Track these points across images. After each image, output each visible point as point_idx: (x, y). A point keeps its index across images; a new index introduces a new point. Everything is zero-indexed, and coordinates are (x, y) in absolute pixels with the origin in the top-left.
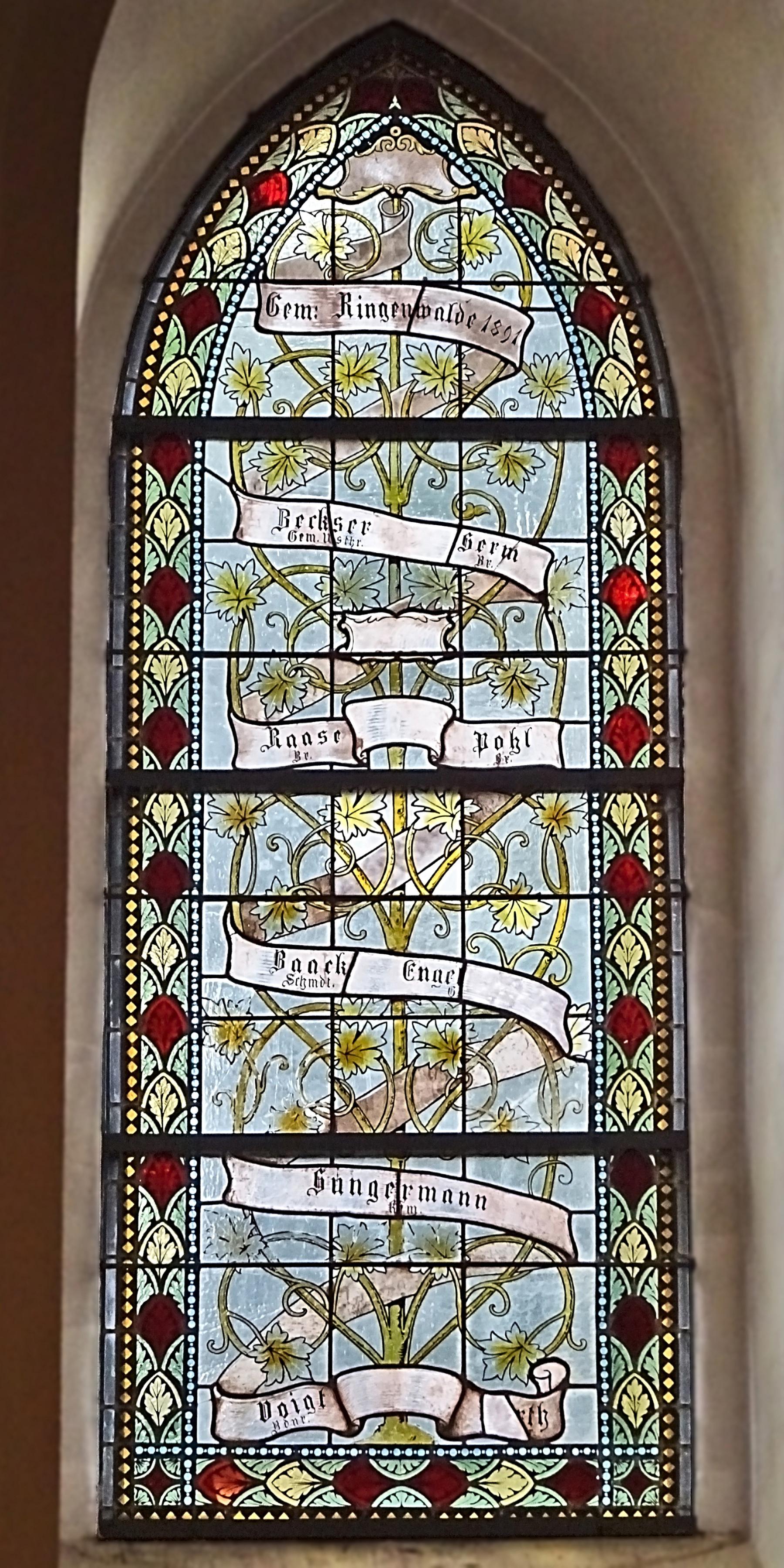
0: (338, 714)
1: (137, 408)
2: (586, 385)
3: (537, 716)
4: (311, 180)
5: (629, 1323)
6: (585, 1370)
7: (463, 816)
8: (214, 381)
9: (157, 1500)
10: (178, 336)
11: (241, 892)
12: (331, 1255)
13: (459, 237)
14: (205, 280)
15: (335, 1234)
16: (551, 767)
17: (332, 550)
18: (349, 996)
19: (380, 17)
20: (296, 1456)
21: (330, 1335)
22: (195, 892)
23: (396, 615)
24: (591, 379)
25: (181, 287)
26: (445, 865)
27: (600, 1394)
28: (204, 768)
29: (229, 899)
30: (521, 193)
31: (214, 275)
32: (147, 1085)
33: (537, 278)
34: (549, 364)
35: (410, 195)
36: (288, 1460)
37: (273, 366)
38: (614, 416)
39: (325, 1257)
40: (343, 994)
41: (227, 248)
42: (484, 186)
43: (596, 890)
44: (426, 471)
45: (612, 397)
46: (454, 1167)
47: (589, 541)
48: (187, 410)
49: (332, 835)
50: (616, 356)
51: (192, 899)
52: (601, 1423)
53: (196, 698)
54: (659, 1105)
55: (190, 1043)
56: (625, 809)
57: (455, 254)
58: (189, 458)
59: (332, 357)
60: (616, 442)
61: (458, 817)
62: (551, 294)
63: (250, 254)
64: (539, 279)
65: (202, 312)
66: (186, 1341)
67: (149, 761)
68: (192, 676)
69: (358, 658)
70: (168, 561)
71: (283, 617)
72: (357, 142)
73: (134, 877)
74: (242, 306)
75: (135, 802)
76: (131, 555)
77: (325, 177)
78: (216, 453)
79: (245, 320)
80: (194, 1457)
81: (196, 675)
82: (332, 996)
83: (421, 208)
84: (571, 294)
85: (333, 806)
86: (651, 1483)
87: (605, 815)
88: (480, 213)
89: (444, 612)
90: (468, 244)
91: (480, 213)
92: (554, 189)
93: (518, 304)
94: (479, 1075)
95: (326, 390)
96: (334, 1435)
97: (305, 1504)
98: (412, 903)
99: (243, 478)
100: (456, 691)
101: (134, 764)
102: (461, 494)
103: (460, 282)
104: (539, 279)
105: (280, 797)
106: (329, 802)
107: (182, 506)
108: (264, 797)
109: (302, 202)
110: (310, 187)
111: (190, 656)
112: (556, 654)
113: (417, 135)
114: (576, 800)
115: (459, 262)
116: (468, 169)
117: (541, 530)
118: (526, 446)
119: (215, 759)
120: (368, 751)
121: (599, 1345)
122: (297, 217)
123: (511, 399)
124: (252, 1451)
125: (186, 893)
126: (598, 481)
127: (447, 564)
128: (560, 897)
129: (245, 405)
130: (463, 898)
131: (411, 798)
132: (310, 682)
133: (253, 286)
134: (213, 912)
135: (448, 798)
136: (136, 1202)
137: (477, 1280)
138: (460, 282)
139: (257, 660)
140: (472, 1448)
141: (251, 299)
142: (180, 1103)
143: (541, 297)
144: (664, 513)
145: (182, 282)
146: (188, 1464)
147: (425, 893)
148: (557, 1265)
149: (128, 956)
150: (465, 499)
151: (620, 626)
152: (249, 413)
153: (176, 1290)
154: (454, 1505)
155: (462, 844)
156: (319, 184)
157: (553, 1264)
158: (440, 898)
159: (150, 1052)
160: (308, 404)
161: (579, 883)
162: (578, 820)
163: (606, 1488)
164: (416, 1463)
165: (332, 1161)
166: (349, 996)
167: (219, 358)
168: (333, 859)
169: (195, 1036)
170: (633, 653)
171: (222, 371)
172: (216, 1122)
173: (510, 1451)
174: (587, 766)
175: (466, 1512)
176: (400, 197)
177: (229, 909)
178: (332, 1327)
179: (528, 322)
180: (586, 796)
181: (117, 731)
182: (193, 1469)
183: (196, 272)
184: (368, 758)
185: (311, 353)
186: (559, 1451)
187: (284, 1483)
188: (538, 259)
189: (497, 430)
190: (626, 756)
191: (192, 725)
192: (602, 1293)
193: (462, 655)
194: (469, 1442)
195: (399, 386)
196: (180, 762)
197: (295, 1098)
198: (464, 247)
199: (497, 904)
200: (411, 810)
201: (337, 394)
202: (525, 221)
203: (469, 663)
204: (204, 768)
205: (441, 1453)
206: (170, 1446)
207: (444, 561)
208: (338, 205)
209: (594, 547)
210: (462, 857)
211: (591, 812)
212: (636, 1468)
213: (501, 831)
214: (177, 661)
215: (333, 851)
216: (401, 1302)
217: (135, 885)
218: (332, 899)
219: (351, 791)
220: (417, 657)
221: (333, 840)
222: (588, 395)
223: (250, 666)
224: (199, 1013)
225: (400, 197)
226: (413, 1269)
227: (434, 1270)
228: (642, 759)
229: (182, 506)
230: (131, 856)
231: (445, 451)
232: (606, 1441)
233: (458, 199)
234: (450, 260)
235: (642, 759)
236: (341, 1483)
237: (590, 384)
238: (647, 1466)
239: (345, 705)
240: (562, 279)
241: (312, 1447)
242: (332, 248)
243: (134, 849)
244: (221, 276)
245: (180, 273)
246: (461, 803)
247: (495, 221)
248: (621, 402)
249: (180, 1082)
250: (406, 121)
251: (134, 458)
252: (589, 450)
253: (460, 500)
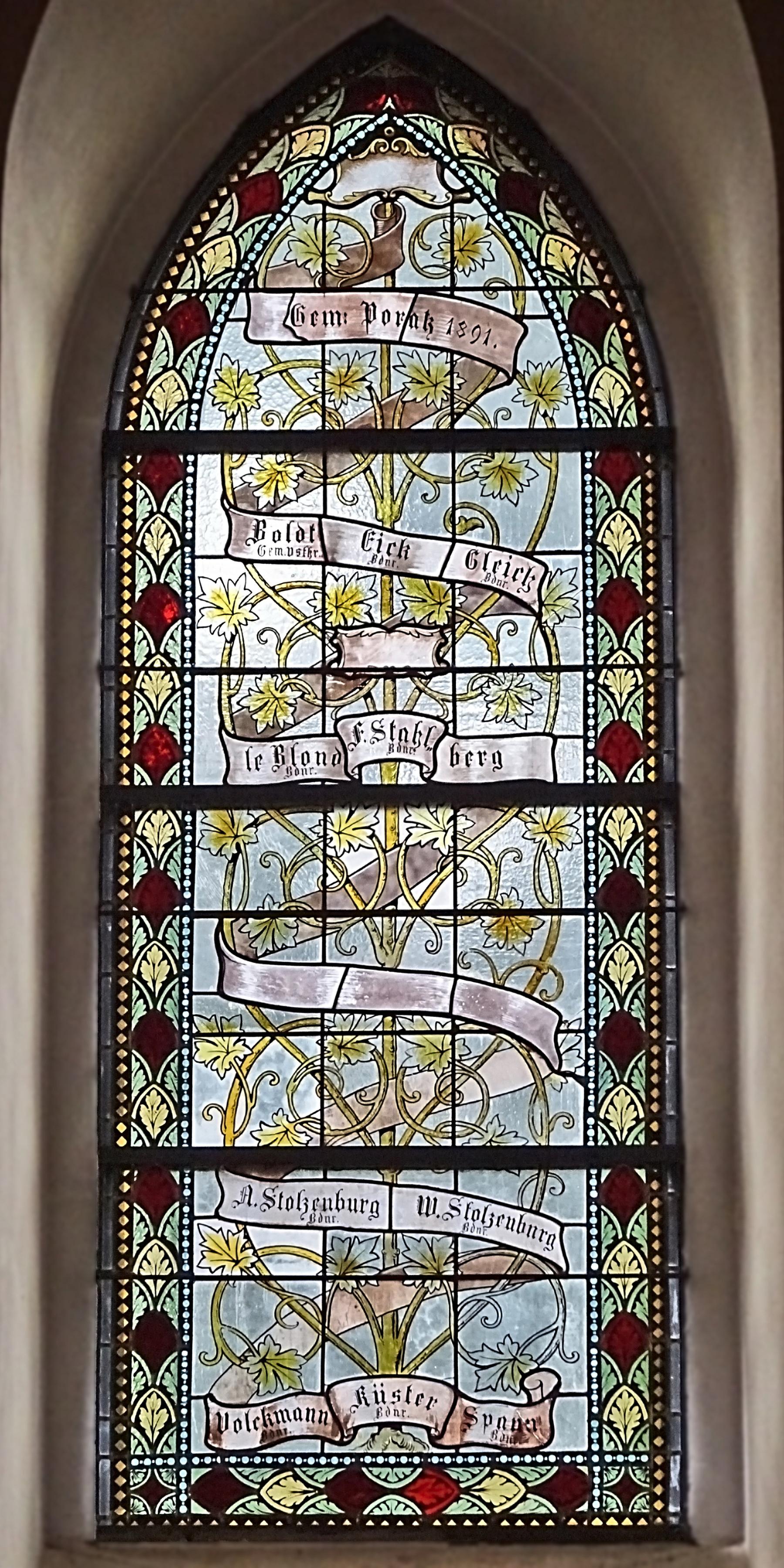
0: (330, 729)
1: (126, 421)
2: (580, 394)
3: (529, 731)
4: (300, 184)
5: (620, 1340)
6: (575, 1379)
7: (455, 832)
8: (202, 392)
9: (153, 1510)
10: (167, 349)
11: (234, 908)
12: (325, 1267)
13: (452, 242)
14: (193, 291)
15: (328, 1248)
16: (544, 782)
17: (324, 564)
18: (341, 1012)
19: (371, 19)
20: (289, 1466)
21: (323, 1346)
22: (186, 908)
23: (390, 631)
24: (586, 389)
25: (169, 300)
26: (438, 881)
27: (591, 1404)
28: (195, 783)
29: (220, 915)
30: (514, 197)
31: (204, 283)
32: (138, 1252)
33: (530, 283)
34: (550, 374)
35: (403, 200)
36: (283, 1468)
37: (262, 378)
38: (609, 425)
39: (316, 1270)
40: (334, 1010)
41: (217, 257)
42: (478, 190)
43: (591, 906)
44: (421, 486)
45: (607, 406)
46: (446, 1180)
47: (583, 553)
48: (175, 423)
49: (324, 850)
50: (611, 365)
51: (183, 914)
52: (590, 1430)
53: (187, 714)
54: (655, 1420)
55: (181, 1058)
56: (621, 824)
57: (448, 258)
58: (181, 474)
59: (323, 367)
60: (612, 454)
61: (451, 833)
62: (545, 302)
63: (239, 263)
64: (532, 284)
65: (192, 324)
66: (180, 982)
67: (141, 777)
68: (184, 690)
69: (350, 674)
70: (155, 1305)
71: (276, 632)
72: (351, 142)
73: (126, 608)
74: (231, 316)
75: (127, 820)
76: (121, 574)
77: (315, 180)
78: (208, 465)
79: (234, 330)
80: (189, 1467)
81: (185, 979)
82: (323, 1011)
83: (414, 215)
84: (566, 299)
85: (325, 821)
86: (641, 1489)
87: (601, 830)
88: (473, 219)
89: (436, 627)
90: (461, 250)
91: (473, 219)
92: (548, 193)
93: (512, 312)
94: (470, 1090)
95: (315, 401)
96: (326, 1444)
97: (299, 1512)
98: (403, 919)
99: (232, 721)
100: (450, 706)
101: (126, 782)
102: (454, 509)
103: (453, 288)
104: (532, 284)
105: (272, 812)
106: (321, 816)
107: (168, 1395)
108: (257, 813)
109: (293, 207)
110: (300, 191)
111: (181, 672)
112: (550, 668)
113: (411, 137)
114: (570, 814)
115: (452, 268)
116: (462, 173)
117: (536, 539)
118: (520, 456)
119: (207, 771)
120: (360, 767)
121: (590, 1356)
122: (287, 222)
123: (506, 408)
124: (245, 1460)
125: (177, 909)
126: (595, 705)
127: (440, 578)
128: (551, 912)
129: (233, 417)
130: (455, 912)
131: (403, 814)
132: (302, 697)
133: (242, 295)
134: (205, 928)
135: (440, 815)
136: (132, 635)
137: (470, 1293)
138: (453, 288)
139: (246, 677)
140: (465, 1455)
141: (240, 310)
142: (170, 1418)
143: (533, 303)
144: (659, 533)
145: (169, 295)
146: (183, 1473)
147: (416, 907)
148: (549, 1277)
149: (120, 974)
150: (458, 513)
151: (615, 639)
152: (238, 427)
153: (171, 1308)
154: (447, 1512)
155: (455, 860)
156: (310, 188)
157: (544, 1277)
158: (434, 913)
159: (142, 1219)
160: (300, 415)
161: (575, 898)
162: (573, 836)
163: (596, 1493)
164: (407, 1471)
165: (325, 1174)
166: (341, 1012)
167: (208, 369)
168: (325, 875)
169: (188, 621)
170: (630, 667)
171: (210, 384)
172: (206, 1134)
173: (504, 1459)
174: (580, 1143)
175: (460, 1519)
176: (392, 200)
177: (221, 924)
178: (325, 1339)
179: (522, 330)
180: (581, 811)
181: (104, 1510)
182: (188, 1479)
183: (185, 284)
184: (360, 774)
185: (304, 363)
186: (552, 1459)
187: (277, 1493)
188: (532, 265)
189: (492, 440)
190: (620, 771)
191: (183, 741)
192: (594, 1305)
193: (455, 671)
194: (462, 1450)
195: (389, 395)
196: (171, 777)
197: (289, 1112)
198: (456, 253)
199: (488, 920)
200: (403, 827)
201: (327, 404)
202: (520, 226)
203: (462, 679)
204: (195, 783)
205: (435, 1460)
206: (166, 1457)
207: (437, 574)
208: (329, 210)
209: (589, 560)
210: (455, 872)
211: (587, 828)
212: (627, 1474)
213: (495, 846)
214: (168, 677)
215: (325, 867)
217: (128, 616)
218: (324, 913)
219: (343, 807)
220: (411, 672)
221: (325, 856)
222: (582, 404)
223: (239, 684)
224: (190, 1029)
225: (392, 200)
226: (407, 1282)
227: (428, 1283)
228: (637, 775)
229: (168, 1395)
230: (125, 490)
231: (436, 463)
232: (595, 1447)
233: (451, 205)
234: (443, 267)
235: (637, 775)
236: (333, 1490)
237: (583, 388)
238: (637, 1472)
239: (337, 721)
240: (558, 284)
241: (305, 1456)
242: (323, 255)
243: (126, 724)
244: (210, 287)
245: (168, 285)
246: (454, 818)
247: (488, 228)
248: (616, 410)
249: (170, 1246)
250: (400, 122)
251: (125, 476)
252: (584, 460)
253: (453, 515)
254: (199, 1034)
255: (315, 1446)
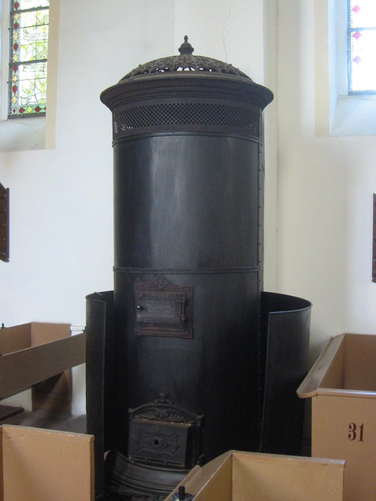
216: (44, 83)
254: (21, 45)
255: (34, 103)
